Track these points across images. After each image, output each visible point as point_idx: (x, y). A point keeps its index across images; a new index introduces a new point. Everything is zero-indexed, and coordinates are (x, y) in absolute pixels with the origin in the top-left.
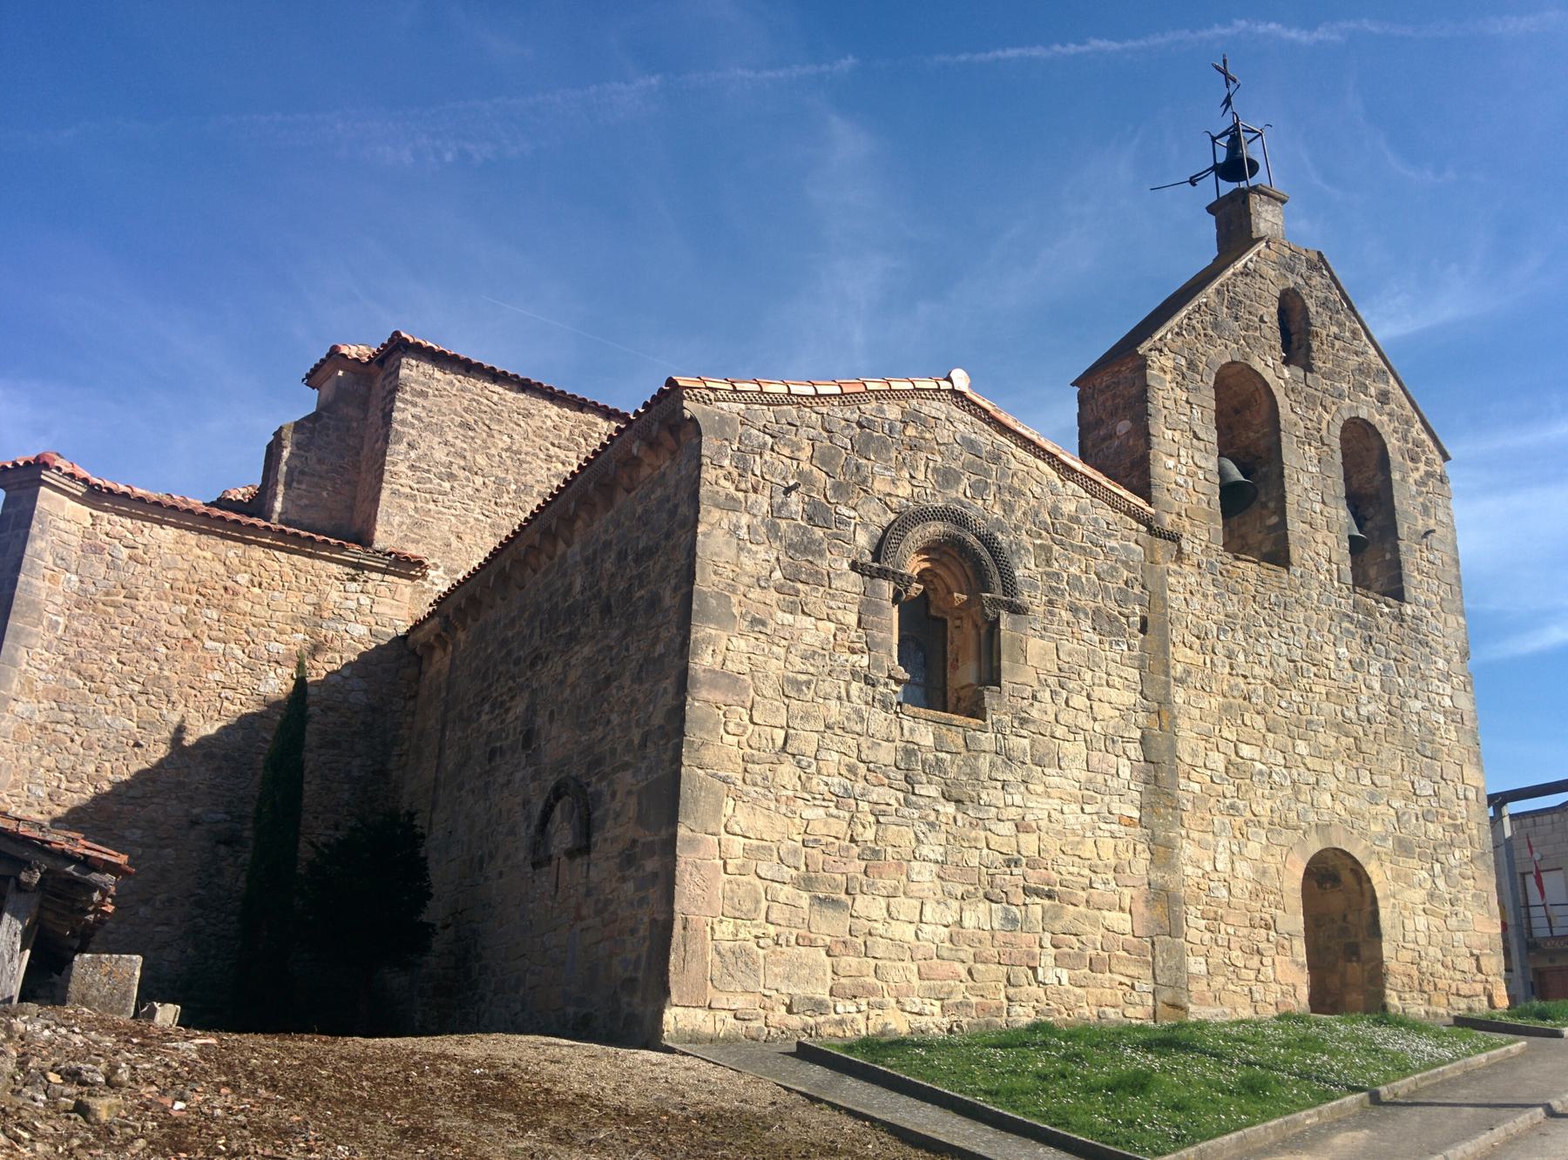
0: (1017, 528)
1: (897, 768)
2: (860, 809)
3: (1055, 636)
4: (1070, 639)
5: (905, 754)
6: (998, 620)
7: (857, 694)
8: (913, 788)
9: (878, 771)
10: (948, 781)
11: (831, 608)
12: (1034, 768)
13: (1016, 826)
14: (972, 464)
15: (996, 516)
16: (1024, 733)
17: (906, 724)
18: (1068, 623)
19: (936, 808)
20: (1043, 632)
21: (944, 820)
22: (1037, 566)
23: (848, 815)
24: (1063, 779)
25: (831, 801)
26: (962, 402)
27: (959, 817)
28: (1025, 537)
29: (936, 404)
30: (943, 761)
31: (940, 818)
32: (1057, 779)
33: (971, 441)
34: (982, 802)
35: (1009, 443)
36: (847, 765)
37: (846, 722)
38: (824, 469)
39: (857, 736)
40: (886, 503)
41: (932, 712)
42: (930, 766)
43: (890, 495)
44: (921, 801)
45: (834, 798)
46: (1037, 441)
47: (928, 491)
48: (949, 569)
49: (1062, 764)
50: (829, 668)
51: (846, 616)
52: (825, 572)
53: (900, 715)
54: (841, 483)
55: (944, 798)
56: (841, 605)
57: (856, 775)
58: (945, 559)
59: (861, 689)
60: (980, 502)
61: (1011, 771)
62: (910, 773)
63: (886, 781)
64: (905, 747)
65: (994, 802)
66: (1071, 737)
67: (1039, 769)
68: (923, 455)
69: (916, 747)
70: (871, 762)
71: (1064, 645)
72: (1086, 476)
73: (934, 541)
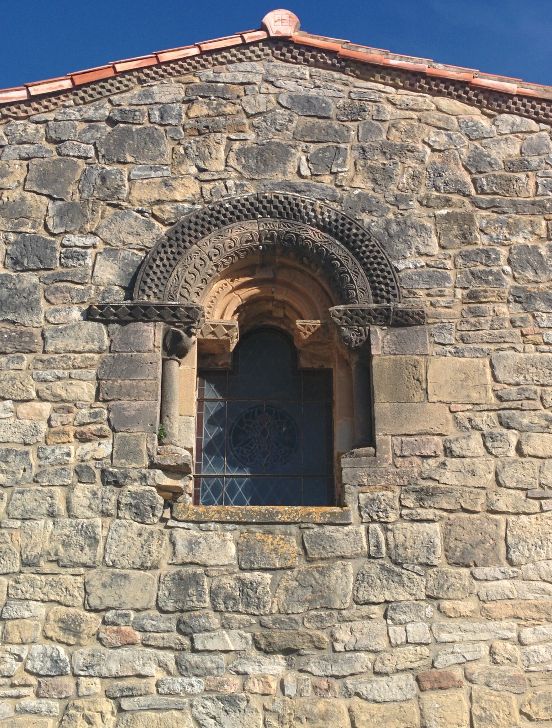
0: (398, 201)
1: (161, 611)
2: (83, 690)
3: (485, 347)
4: (519, 347)
5: (178, 585)
6: (368, 343)
7: (86, 502)
8: (192, 640)
9: (120, 621)
10: (267, 620)
11: (46, 381)
12: (452, 570)
13: (417, 680)
14: (310, 130)
15: (357, 192)
16: (429, 514)
17: (181, 536)
18: (512, 322)
19: (240, 669)
20: (461, 345)
21: (258, 688)
22: (443, 247)
23: (56, 706)
24: (519, 583)
25: (29, 686)
26: (290, 51)
27: (290, 679)
28: (416, 209)
29: (247, 65)
30: (253, 586)
31: (250, 685)
32: (507, 583)
33: (308, 99)
34: (339, 647)
35: (381, 87)
36: (61, 621)
37: (61, 550)
38: (45, 192)
39: (82, 570)
40: (154, 216)
41: (231, 508)
42: (228, 597)
43: (159, 202)
44: (208, 661)
45: (33, 680)
46: (428, 71)
47: (230, 183)
48: (295, 290)
49: (514, 556)
50: (35, 470)
51: (69, 388)
52: (37, 332)
53: (171, 523)
54: (73, 204)
55: (259, 649)
56: (60, 373)
57: (77, 634)
58: (283, 276)
59: (95, 494)
60: (327, 179)
61: (401, 583)
62: (186, 616)
63: (139, 636)
64: (178, 573)
65: (364, 642)
66: (534, 505)
67: (465, 571)
68: (222, 137)
69: (200, 570)
70: (108, 609)
71: (506, 358)
72: (531, 98)
73: (249, 252)
